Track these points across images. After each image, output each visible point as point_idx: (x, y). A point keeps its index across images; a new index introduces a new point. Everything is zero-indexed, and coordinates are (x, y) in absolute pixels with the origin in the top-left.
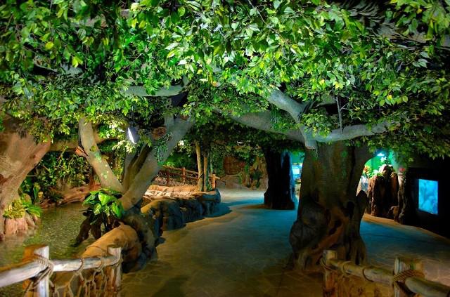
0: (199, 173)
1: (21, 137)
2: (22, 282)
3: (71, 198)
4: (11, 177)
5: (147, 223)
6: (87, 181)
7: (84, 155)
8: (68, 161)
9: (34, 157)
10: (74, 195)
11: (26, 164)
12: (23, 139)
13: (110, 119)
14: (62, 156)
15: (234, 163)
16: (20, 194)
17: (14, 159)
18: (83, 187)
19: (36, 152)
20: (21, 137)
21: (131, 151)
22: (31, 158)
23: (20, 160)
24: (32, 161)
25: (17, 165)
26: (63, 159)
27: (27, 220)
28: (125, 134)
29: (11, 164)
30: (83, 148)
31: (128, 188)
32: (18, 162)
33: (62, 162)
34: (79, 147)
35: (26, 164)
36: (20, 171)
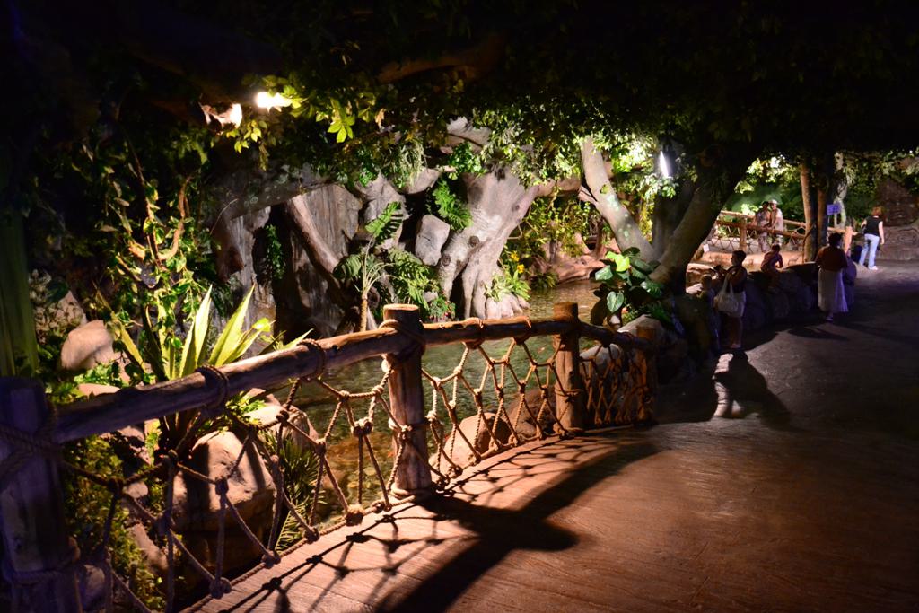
0: (806, 225)
1: (499, 180)
2: (60, 349)
3: (567, 274)
4: (489, 239)
5: (696, 310)
6: (591, 246)
7: (592, 200)
8: (561, 213)
9: (517, 207)
10: (572, 269)
11: (507, 220)
12: (502, 181)
13: (630, 140)
14: (552, 204)
15: (901, 200)
16: (499, 265)
17: (491, 213)
18: (586, 257)
19: (519, 200)
20: (499, 180)
21: (674, 193)
22: (513, 210)
23: (499, 213)
24: (515, 213)
25: (496, 222)
26: (554, 209)
27: (511, 303)
28: (655, 161)
29: (488, 221)
30: (589, 190)
31: (663, 252)
32: (497, 218)
33: (553, 215)
34: (583, 189)
35: (507, 219)
36: (500, 231)
